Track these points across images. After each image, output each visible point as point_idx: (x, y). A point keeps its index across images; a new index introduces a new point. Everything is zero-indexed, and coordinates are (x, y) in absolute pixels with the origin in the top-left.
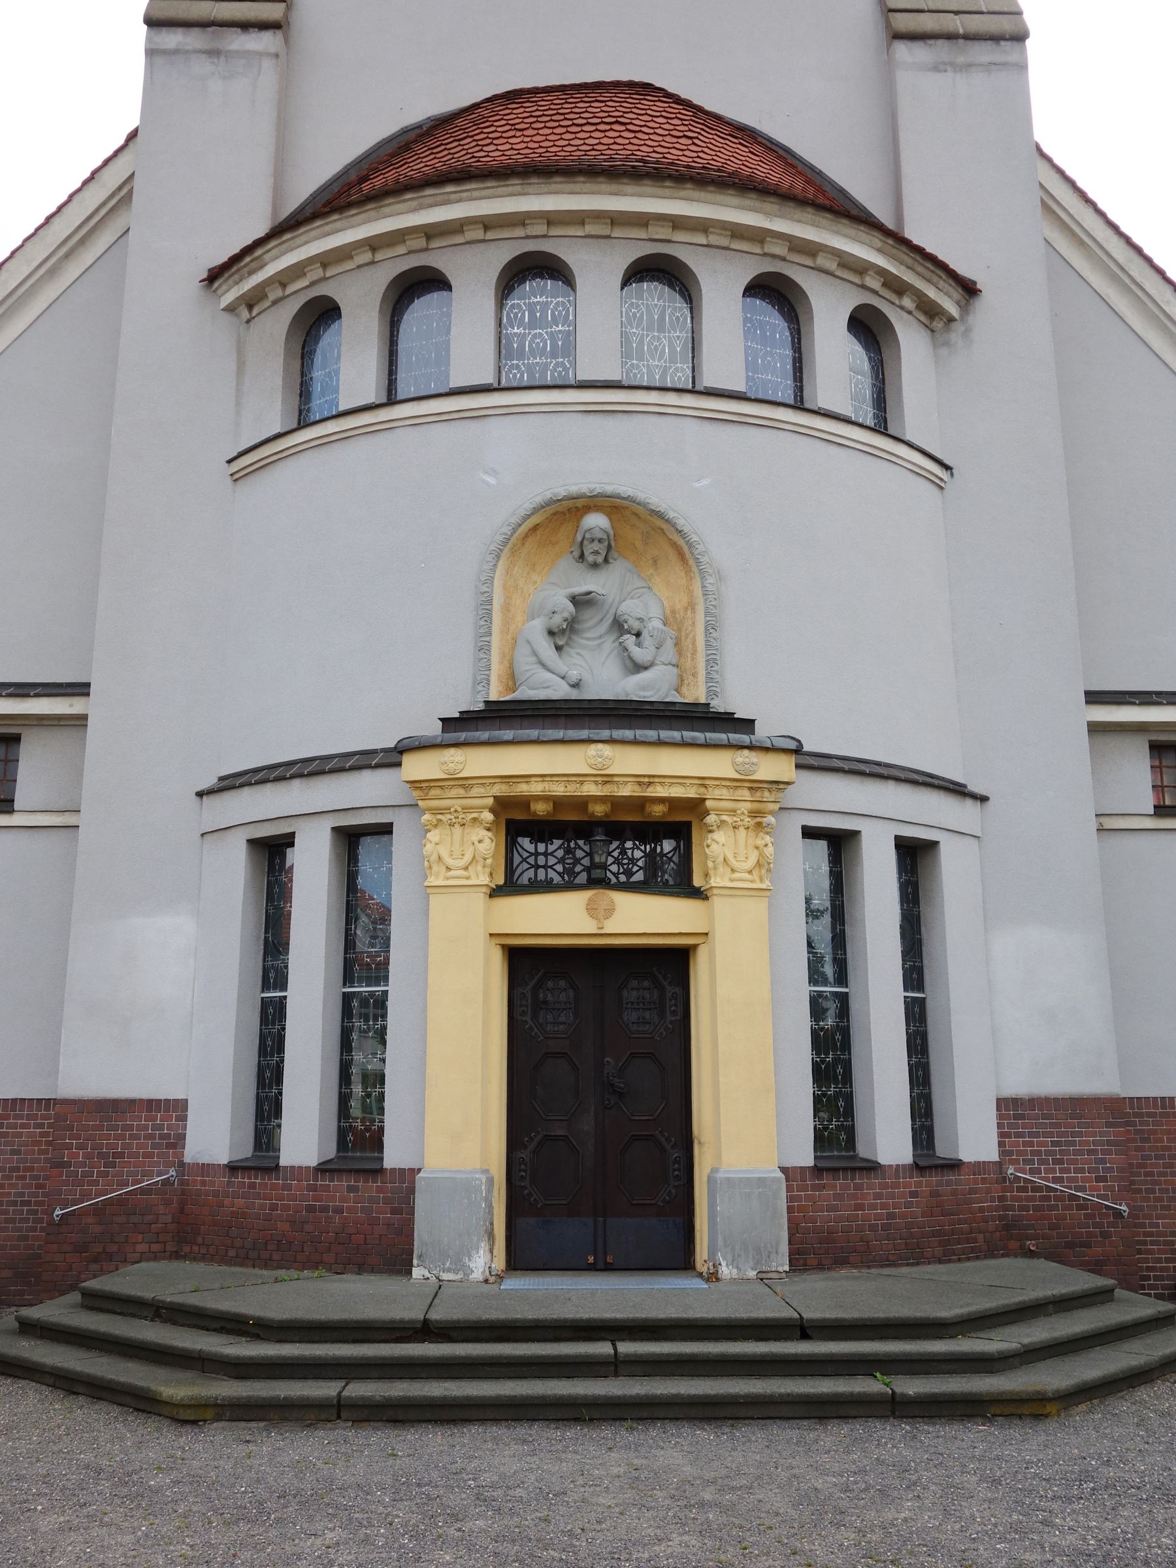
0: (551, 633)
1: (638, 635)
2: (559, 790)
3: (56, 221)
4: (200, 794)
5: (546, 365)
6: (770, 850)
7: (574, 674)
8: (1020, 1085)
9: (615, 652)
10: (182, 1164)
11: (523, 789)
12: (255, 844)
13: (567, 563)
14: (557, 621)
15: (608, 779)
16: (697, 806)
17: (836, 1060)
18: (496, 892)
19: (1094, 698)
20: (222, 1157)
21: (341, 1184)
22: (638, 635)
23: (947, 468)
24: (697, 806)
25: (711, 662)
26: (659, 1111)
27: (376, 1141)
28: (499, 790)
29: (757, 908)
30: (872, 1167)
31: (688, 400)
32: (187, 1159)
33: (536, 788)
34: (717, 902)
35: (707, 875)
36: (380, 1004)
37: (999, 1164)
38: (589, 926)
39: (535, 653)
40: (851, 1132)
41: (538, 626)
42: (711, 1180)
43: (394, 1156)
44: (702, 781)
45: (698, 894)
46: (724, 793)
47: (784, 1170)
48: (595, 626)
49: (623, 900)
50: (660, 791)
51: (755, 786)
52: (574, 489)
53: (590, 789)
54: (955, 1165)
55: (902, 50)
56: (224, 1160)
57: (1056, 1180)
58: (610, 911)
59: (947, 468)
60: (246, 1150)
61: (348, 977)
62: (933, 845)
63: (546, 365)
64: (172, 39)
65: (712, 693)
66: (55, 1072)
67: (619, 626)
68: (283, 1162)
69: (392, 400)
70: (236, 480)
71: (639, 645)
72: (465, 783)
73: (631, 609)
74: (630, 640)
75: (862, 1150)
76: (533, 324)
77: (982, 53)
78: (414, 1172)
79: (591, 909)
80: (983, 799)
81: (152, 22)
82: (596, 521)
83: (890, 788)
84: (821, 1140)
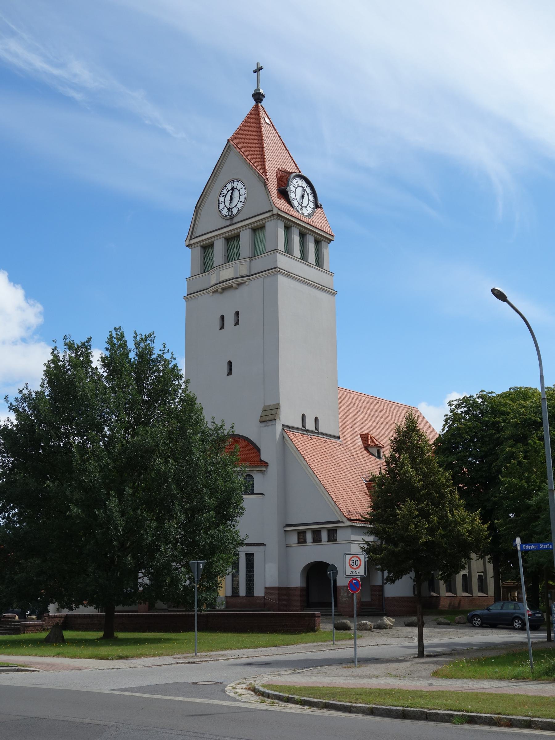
8: (268, 585)
37: (264, 597)
59: (262, 494)
77: (270, 423)
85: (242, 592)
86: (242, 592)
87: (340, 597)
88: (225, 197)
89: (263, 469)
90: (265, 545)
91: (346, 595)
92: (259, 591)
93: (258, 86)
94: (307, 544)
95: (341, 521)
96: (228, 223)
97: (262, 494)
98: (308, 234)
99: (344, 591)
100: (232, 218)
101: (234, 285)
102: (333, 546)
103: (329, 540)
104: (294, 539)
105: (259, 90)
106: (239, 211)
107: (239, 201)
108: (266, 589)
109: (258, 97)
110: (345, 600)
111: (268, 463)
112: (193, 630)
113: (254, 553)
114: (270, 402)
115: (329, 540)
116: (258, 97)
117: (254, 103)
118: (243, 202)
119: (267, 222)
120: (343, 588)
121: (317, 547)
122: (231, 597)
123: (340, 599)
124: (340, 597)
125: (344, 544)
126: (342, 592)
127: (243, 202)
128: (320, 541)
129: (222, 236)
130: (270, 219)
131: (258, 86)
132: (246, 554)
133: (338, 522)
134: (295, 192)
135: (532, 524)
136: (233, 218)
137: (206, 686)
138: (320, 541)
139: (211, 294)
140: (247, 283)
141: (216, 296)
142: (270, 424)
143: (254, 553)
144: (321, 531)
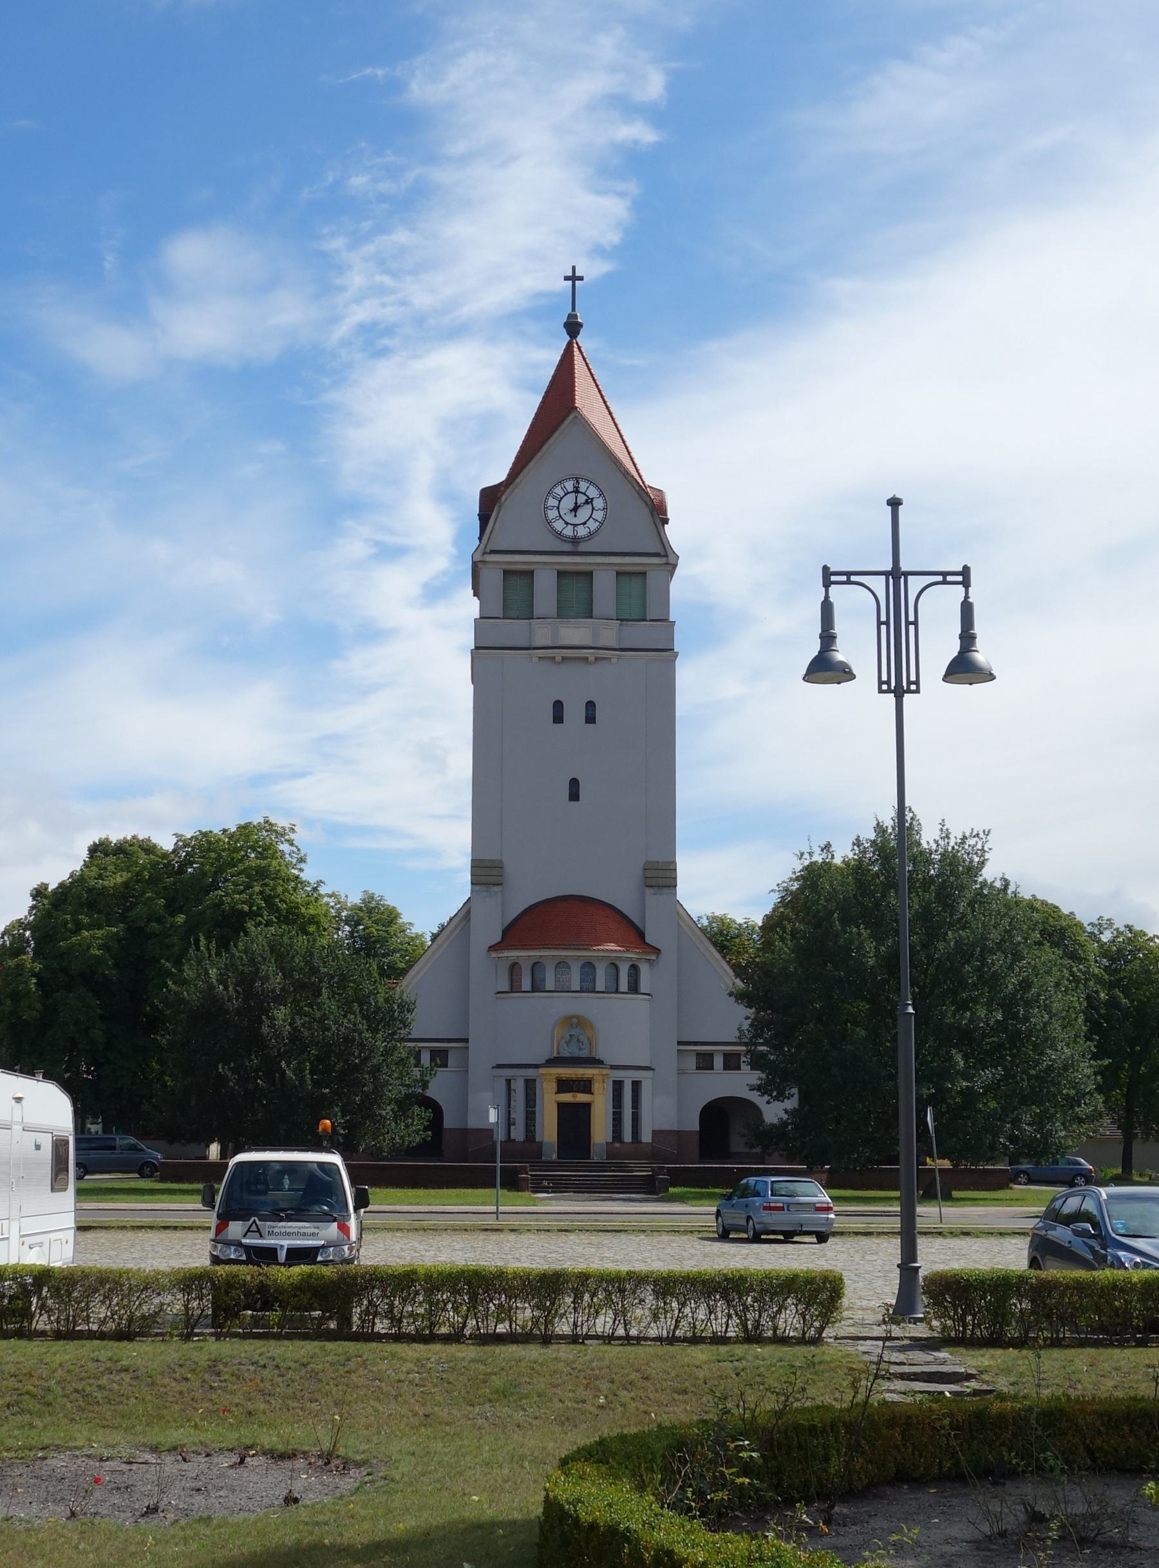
8: (657, 1128)
9: (460, 147)
12: (506, 1080)
18: (556, 1093)
19: (680, 1043)
20: (522, 1140)
23: (649, 994)
26: (628, 1195)
27: (534, 1136)
36: (534, 1113)
40: (620, 1136)
44: (593, 1075)
45: (593, 1094)
49: (579, 1095)
51: (603, 1075)
55: (647, 890)
58: (576, 1097)
61: (527, 1107)
64: (477, 888)
70: (497, 998)
72: (551, 1074)
77: (666, 890)
79: (573, 1096)
85: (627, 1136)
86: (627, 1136)
88: (560, 501)
90: (653, 1070)
92: (646, 1137)
93: (574, 309)
96: (568, 547)
100: (575, 540)
101: (592, 659)
104: (692, 1062)
105: (576, 316)
106: (591, 535)
107: (591, 517)
111: (660, 950)
112: (493, 1186)
113: (623, 1081)
117: (568, 338)
121: (733, 1075)
122: (524, 1141)
131: (574, 309)
134: (558, 508)
135: (355, 1075)
136: (579, 542)
137: (806, 1246)
139: (535, 660)
143: (623, 1081)
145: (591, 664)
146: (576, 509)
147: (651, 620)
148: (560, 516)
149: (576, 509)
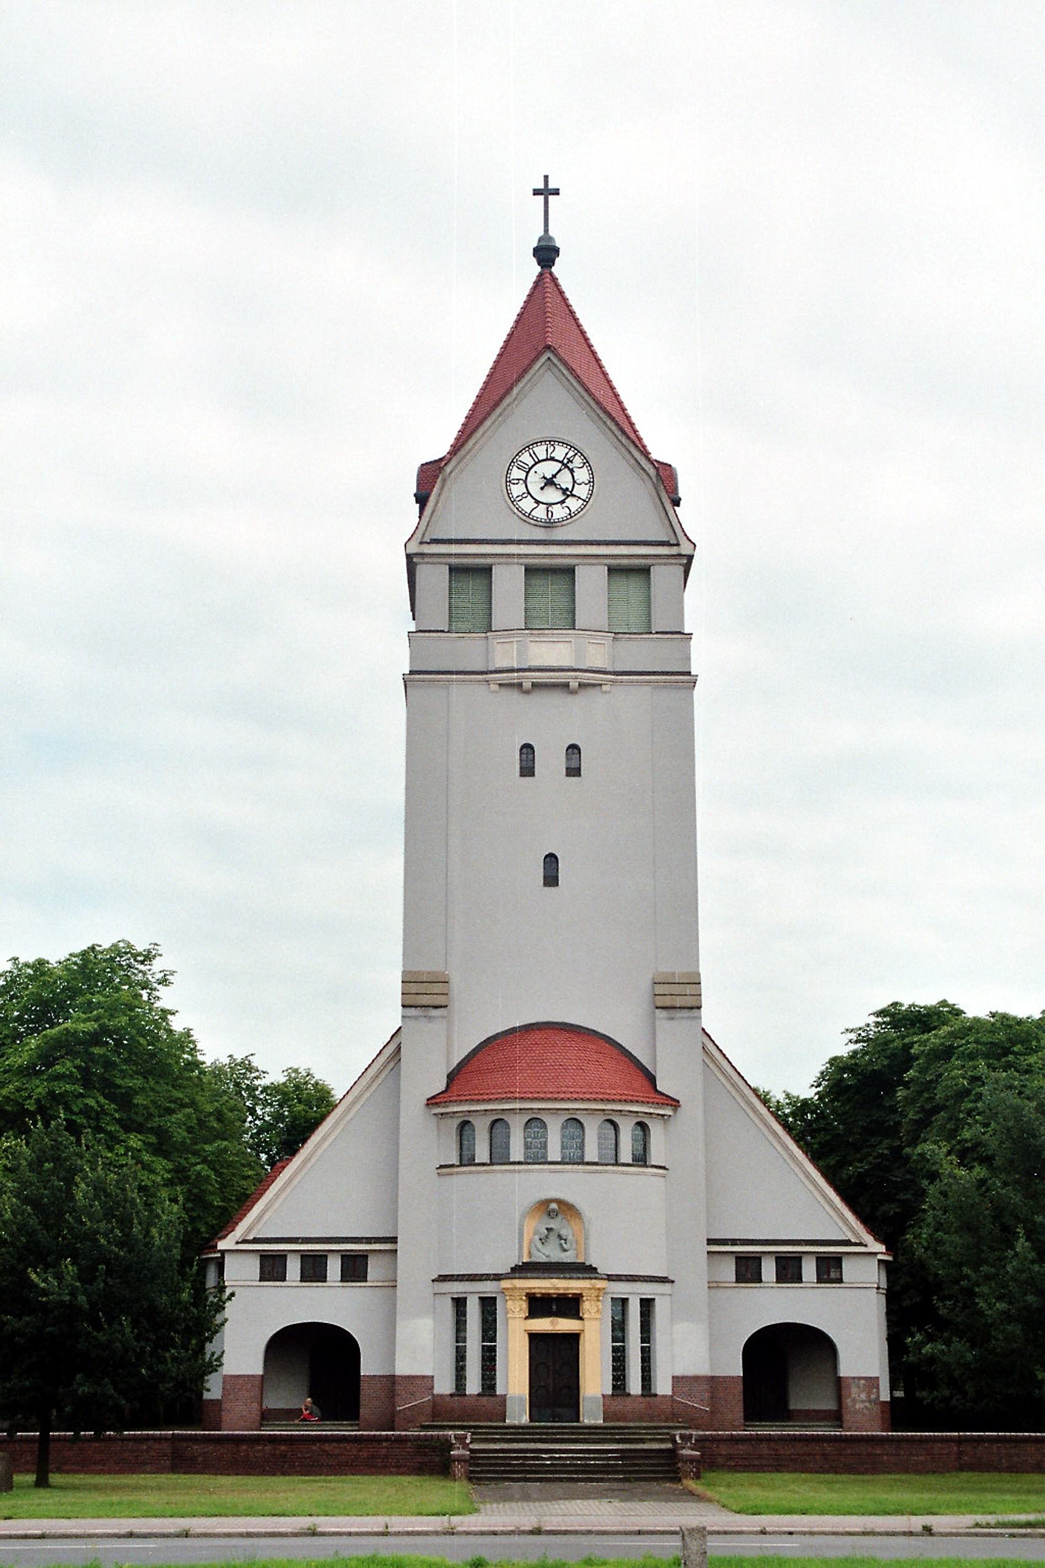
0: (540, 1239)
1: (565, 1240)
2: (543, 1291)
3: (369, 1070)
4: (433, 1281)
5: (538, 1152)
6: (600, 1307)
7: (547, 1254)
10: (433, 1395)
11: (533, 1291)
13: (545, 1217)
14: (543, 1236)
15: (558, 1289)
16: (581, 1295)
17: (621, 1365)
18: (526, 1318)
19: (711, 1242)
21: (484, 1400)
22: (565, 1240)
24: (581, 1295)
25: (586, 1249)
27: (493, 1387)
28: (528, 1291)
29: (597, 1324)
30: (629, 1395)
31: (580, 1167)
32: (435, 1392)
33: (537, 1291)
34: (586, 1322)
35: (583, 1314)
37: (672, 1396)
38: (551, 1328)
39: (536, 1246)
40: (624, 1385)
41: (537, 1237)
42: (583, 1397)
43: (499, 1391)
44: (581, 1289)
45: (581, 1319)
46: (587, 1291)
47: (603, 1395)
48: (553, 1237)
50: (571, 1292)
52: (547, 1197)
53: (552, 1291)
54: (656, 1395)
56: (476, 1393)
57: (689, 1401)
59: (664, 1168)
60: (453, 1391)
62: (653, 1300)
63: (538, 1152)
65: (585, 1259)
66: (394, 1368)
67: (560, 1237)
68: (467, 1393)
69: (491, 1164)
71: (566, 1243)
73: (563, 1232)
74: (563, 1241)
75: (653, 1392)
76: (534, 1138)
78: (505, 1395)
79: (552, 1323)
80: (673, 1282)
81: (403, 1006)
82: (554, 1206)
83: (639, 1284)
84: (614, 1387)
86: (635, 1386)
87: (849, 1401)
89: (668, 1111)
91: (863, 1396)
92: (663, 1387)
94: (843, 1285)
95: (853, 1240)
97: (664, 1168)
98: (495, 564)
99: (859, 1387)
100: (550, 524)
102: (830, 1293)
103: (781, 1278)
104: (728, 1270)
108: (676, 1379)
109: (546, 254)
110: (861, 1406)
111: (678, 1102)
114: (676, 968)
115: (781, 1278)
116: (546, 254)
118: (584, 501)
119: (657, 564)
120: (856, 1381)
121: (314, 1292)
123: (850, 1404)
124: (849, 1401)
125: (859, 1290)
126: (854, 1391)
127: (584, 501)
128: (283, 1279)
129: (521, 561)
130: (673, 561)
132: (641, 1300)
133: (847, 1243)
138: (799, 1279)
140: (604, 688)
141: (514, 695)
142: (678, 1015)
144: (760, 1259)
145: (573, 692)
146: (550, 482)
147: (657, 633)
148: (529, 493)
149: (550, 482)
